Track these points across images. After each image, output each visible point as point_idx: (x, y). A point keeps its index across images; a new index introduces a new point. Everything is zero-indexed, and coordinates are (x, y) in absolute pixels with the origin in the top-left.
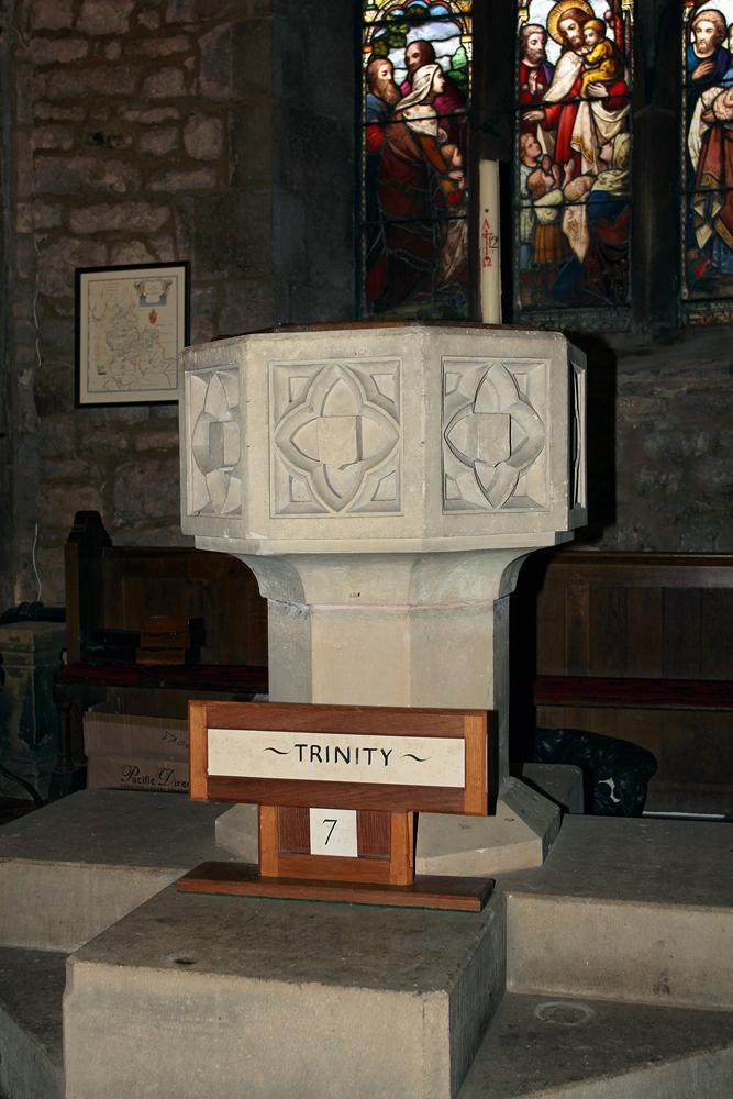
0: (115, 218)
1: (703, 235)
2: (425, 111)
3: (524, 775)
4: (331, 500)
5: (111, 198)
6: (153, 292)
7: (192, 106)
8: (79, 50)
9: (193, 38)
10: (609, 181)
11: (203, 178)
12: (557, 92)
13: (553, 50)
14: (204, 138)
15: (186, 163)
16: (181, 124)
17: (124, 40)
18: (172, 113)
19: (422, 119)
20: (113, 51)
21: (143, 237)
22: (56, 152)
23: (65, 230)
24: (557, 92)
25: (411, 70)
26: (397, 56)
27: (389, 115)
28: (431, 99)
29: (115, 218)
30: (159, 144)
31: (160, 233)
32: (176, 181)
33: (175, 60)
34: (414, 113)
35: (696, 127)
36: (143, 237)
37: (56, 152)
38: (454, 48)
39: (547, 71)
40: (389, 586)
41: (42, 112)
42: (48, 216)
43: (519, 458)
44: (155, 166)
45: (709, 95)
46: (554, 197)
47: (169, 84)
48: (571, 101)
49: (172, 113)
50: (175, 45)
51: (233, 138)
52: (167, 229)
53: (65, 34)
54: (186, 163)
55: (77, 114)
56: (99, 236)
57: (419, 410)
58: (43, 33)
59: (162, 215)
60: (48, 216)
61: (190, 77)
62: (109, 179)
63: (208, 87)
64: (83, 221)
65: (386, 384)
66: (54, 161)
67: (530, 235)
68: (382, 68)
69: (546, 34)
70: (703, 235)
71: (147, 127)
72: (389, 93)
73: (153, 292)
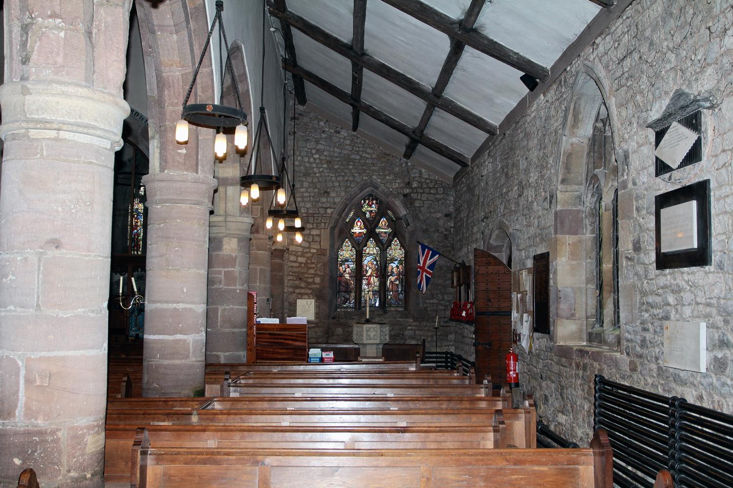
0: (303, 291)
1: (389, 297)
2: (348, 275)
3: (662, 211)
4: (370, 339)
5: (302, 288)
6: (309, 303)
7: (315, 275)
8: (298, 265)
9: (316, 265)
10: (376, 288)
11: (318, 286)
12: (368, 275)
13: (368, 268)
14: (318, 280)
15: (315, 284)
16: (314, 278)
17: (305, 264)
18: (313, 276)
19: (347, 276)
20: (303, 265)
21: (307, 294)
22: (293, 280)
23: (294, 292)
24: (368, 275)
25: (346, 269)
26: (343, 266)
27: (342, 275)
28: (349, 274)
29: (303, 291)
30: (310, 280)
31: (311, 294)
32: (313, 286)
33: (313, 268)
34: (346, 275)
35: (389, 282)
36: (307, 294)
37: (293, 280)
38: (352, 266)
39: (367, 271)
40: (375, 347)
41: (290, 273)
42: (291, 290)
43: (386, 335)
44: (309, 283)
45: (391, 277)
46: (368, 290)
47: (312, 271)
48: (370, 276)
49: (313, 276)
50: (313, 266)
51: (322, 280)
52: (311, 293)
53: (295, 262)
54: (315, 284)
55: (297, 274)
56: (300, 294)
57: (379, 331)
58: (291, 261)
59: (311, 291)
60: (291, 290)
61: (316, 271)
62: (302, 285)
63: (319, 273)
64: (297, 291)
65: (376, 329)
66: (292, 281)
67: (163, 91)
68: (341, 268)
69: (367, 266)
70: (389, 297)
71: (308, 278)
72: (342, 272)
73: (309, 303)
